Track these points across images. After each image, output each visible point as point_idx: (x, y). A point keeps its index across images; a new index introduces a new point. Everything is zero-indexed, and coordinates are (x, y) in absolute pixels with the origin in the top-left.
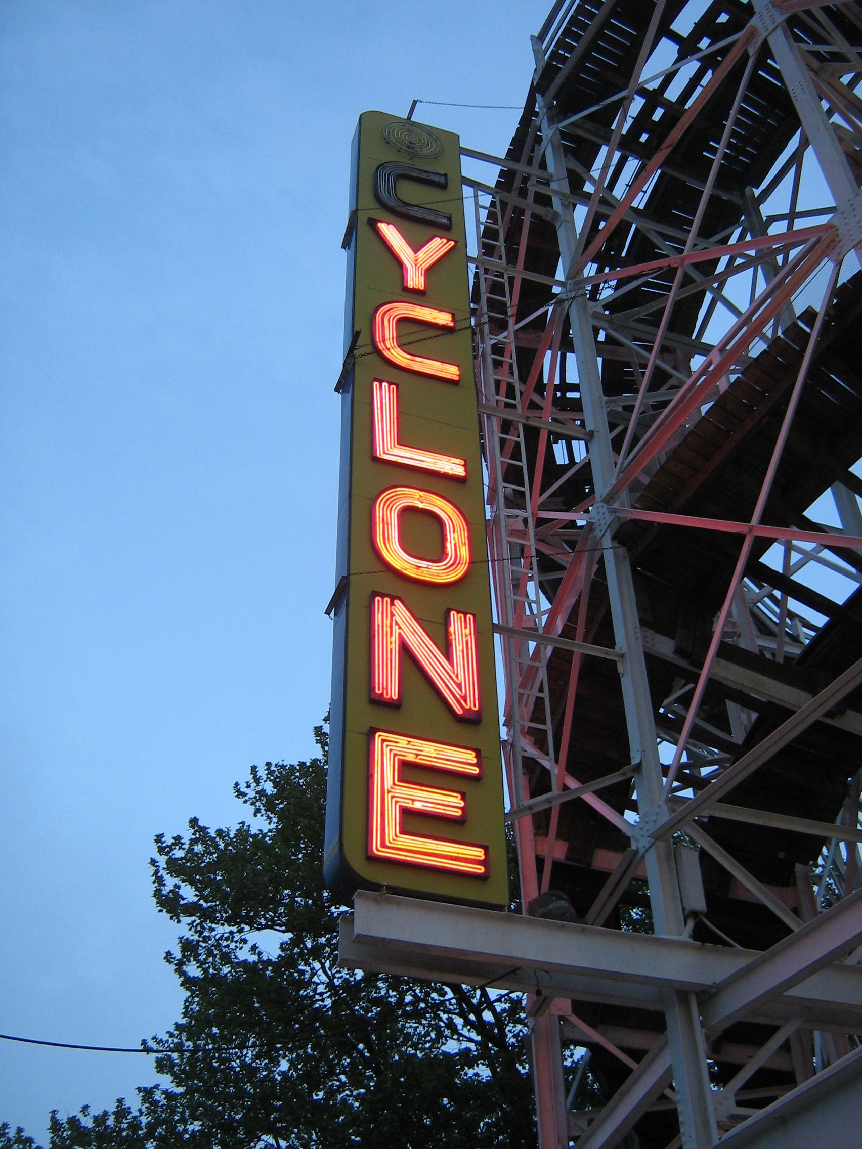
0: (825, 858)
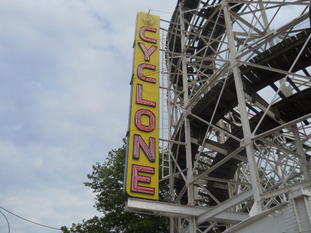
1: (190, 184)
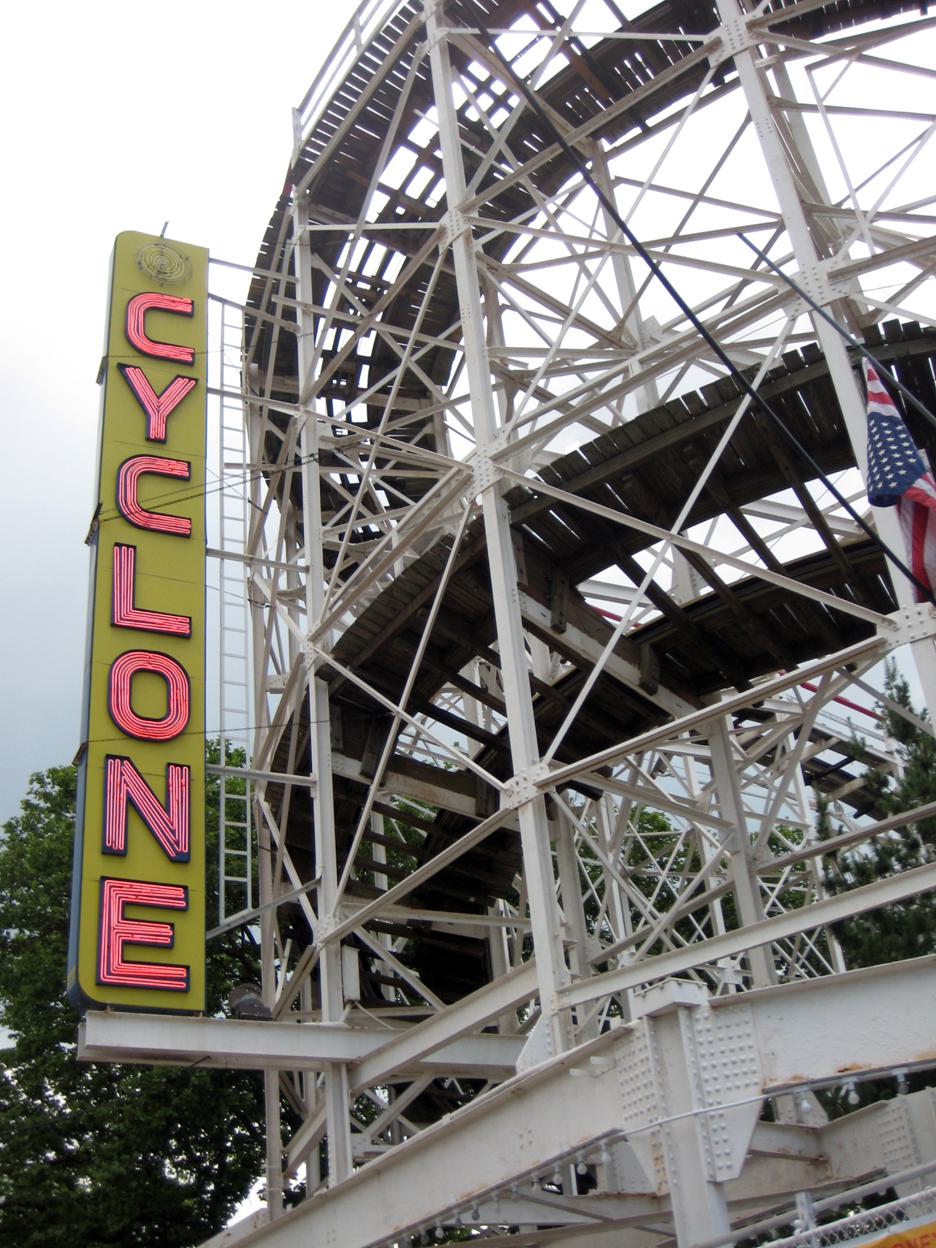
0: (717, 717)
1: (327, 942)
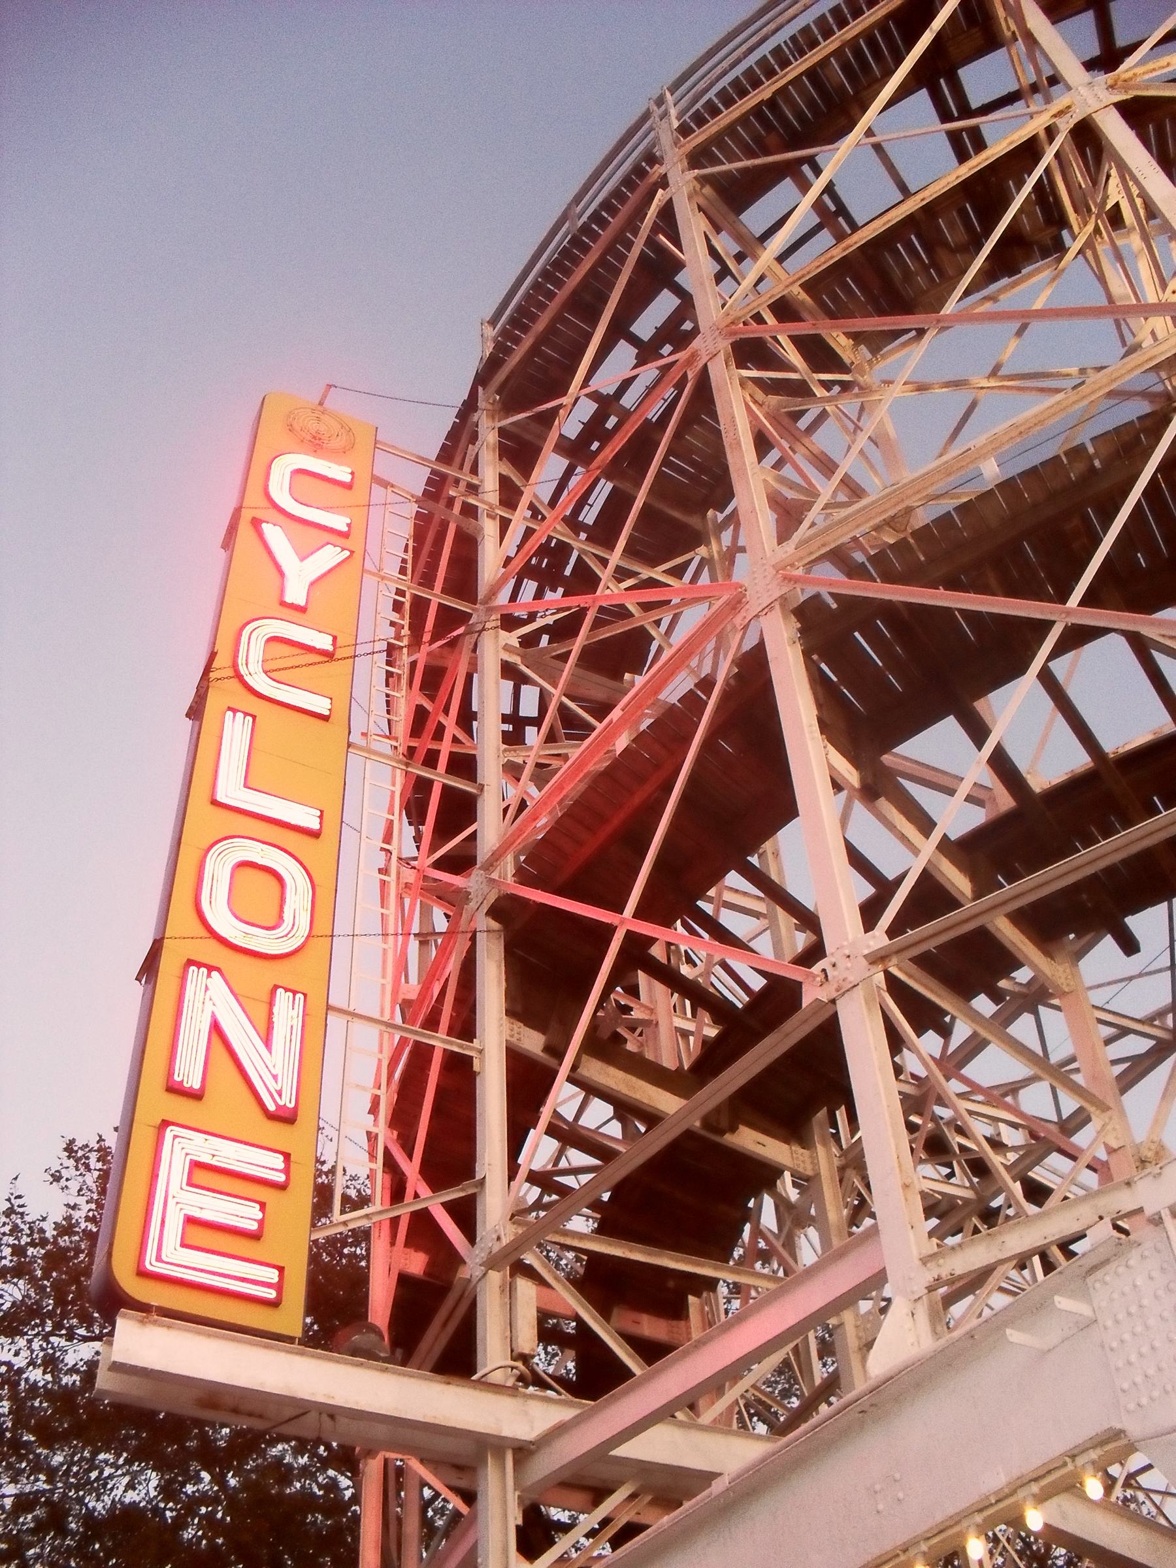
1: (492, 1263)
